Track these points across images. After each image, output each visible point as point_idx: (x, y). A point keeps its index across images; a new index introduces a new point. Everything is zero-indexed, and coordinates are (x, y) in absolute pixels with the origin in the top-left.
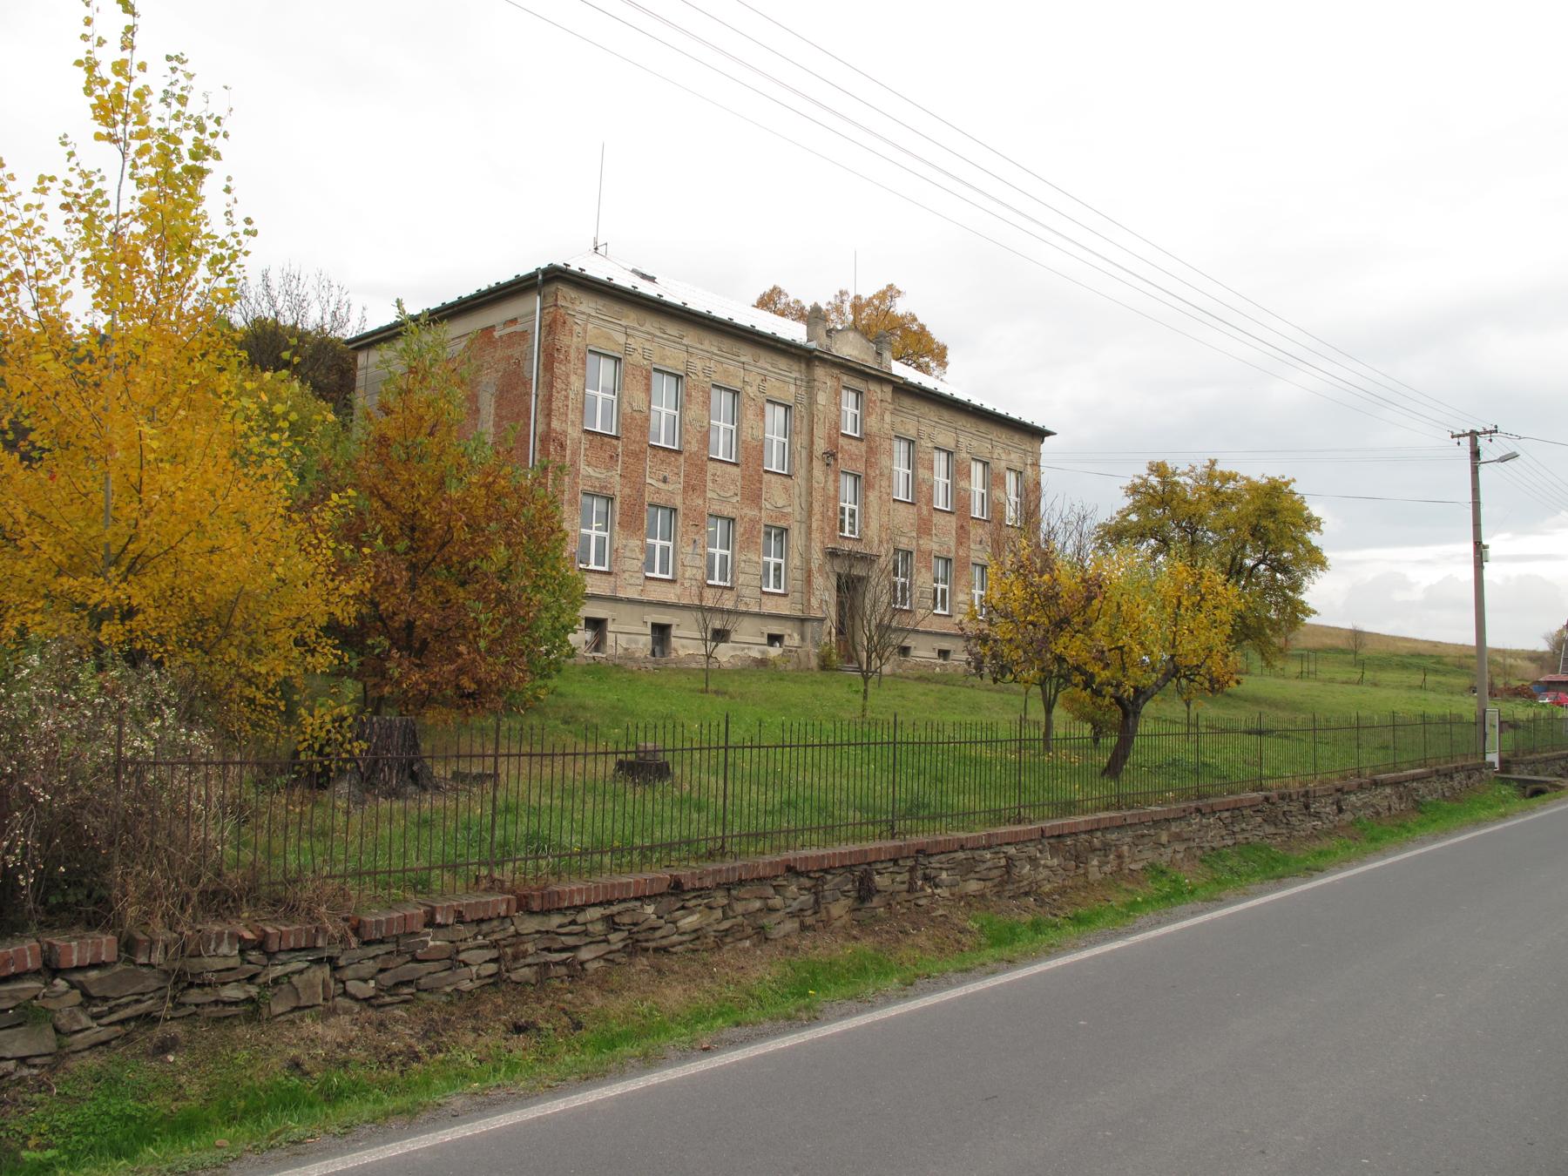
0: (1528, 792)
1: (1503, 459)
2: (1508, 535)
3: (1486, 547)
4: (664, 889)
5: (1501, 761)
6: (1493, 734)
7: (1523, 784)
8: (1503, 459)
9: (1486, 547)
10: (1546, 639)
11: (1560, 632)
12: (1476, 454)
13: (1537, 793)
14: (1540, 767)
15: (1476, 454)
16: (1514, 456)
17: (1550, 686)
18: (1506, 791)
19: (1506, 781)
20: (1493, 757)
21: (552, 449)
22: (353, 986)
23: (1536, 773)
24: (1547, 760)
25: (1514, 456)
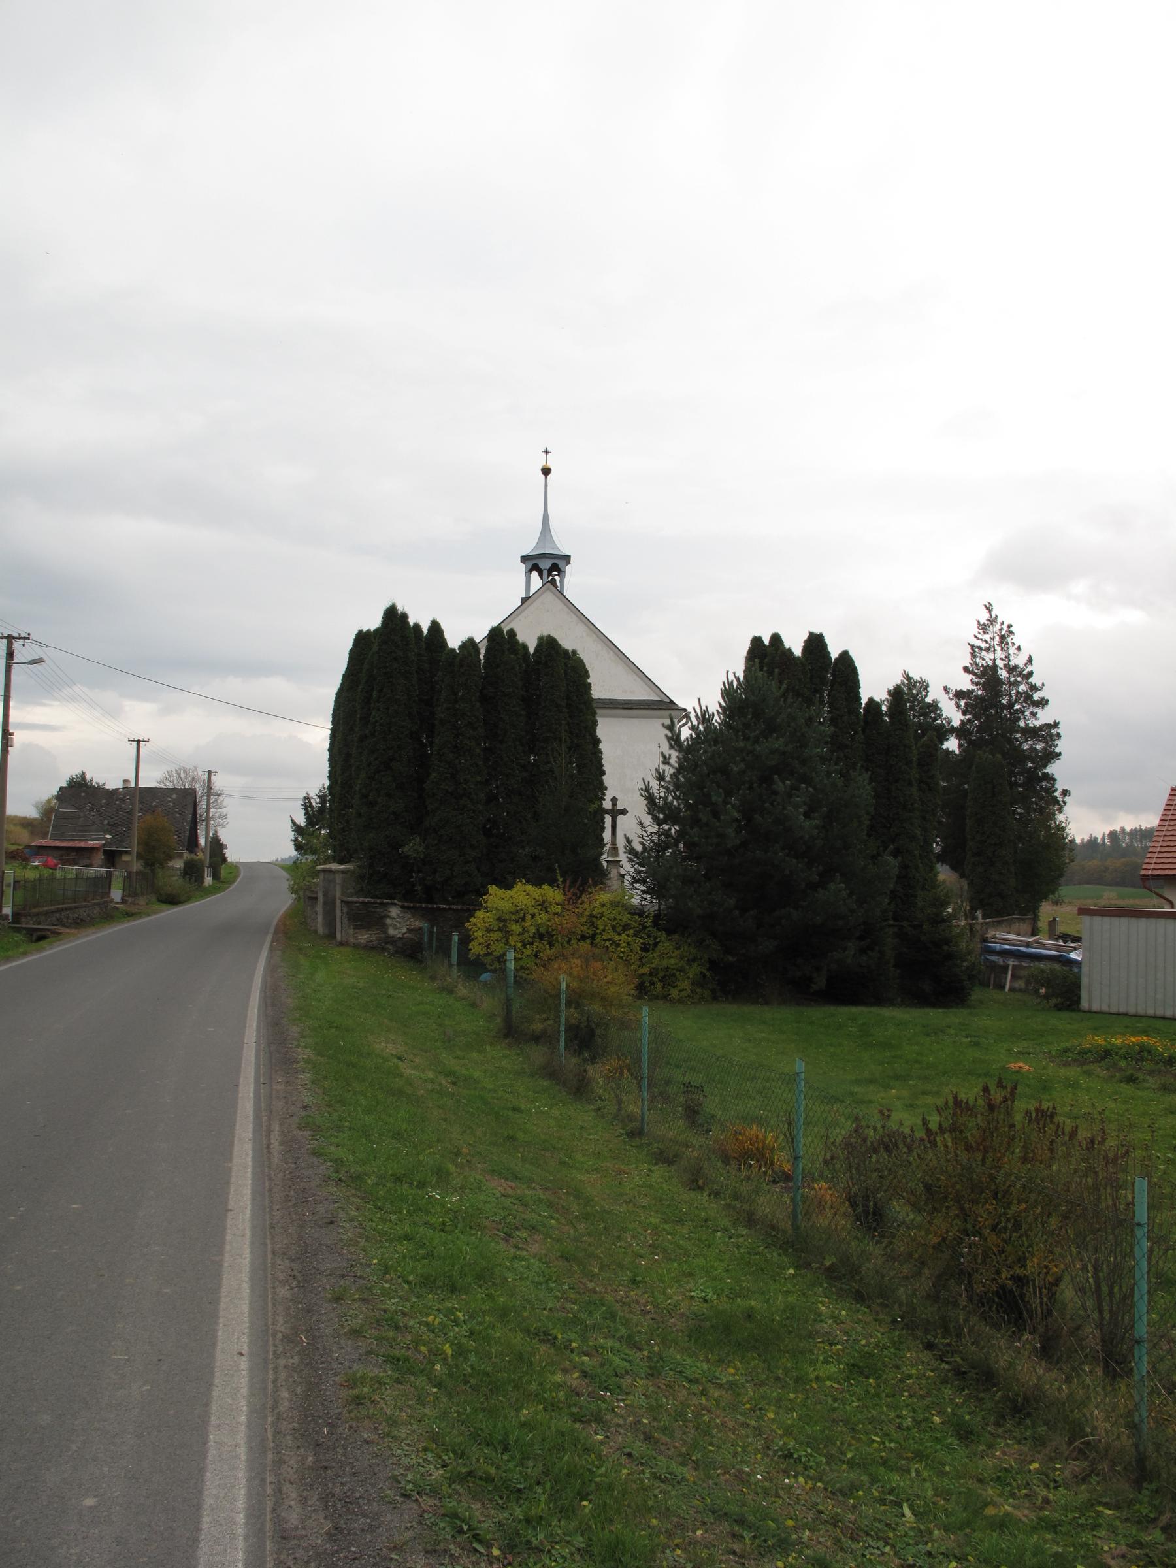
0: (34, 938)
1: (32, 663)
2: (107, 787)
3: (12, 734)
4: (1142, 1449)
5: (14, 914)
6: (9, 892)
7: (31, 931)
8: (32, 663)
9: (12, 734)
10: (37, 807)
11: (49, 801)
12: (10, 655)
13: (41, 938)
14: (43, 918)
15: (10, 655)
16: (40, 661)
17: (40, 850)
18: (18, 937)
19: (18, 930)
20: (7, 911)
21: (1148, 1538)
22: (1137, 1398)
23: (39, 923)
24: (47, 913)
25: (40, 661)
